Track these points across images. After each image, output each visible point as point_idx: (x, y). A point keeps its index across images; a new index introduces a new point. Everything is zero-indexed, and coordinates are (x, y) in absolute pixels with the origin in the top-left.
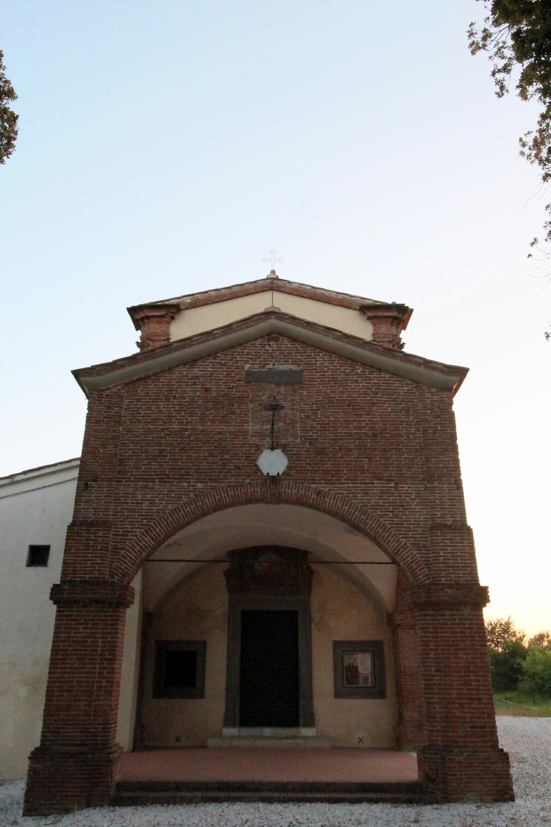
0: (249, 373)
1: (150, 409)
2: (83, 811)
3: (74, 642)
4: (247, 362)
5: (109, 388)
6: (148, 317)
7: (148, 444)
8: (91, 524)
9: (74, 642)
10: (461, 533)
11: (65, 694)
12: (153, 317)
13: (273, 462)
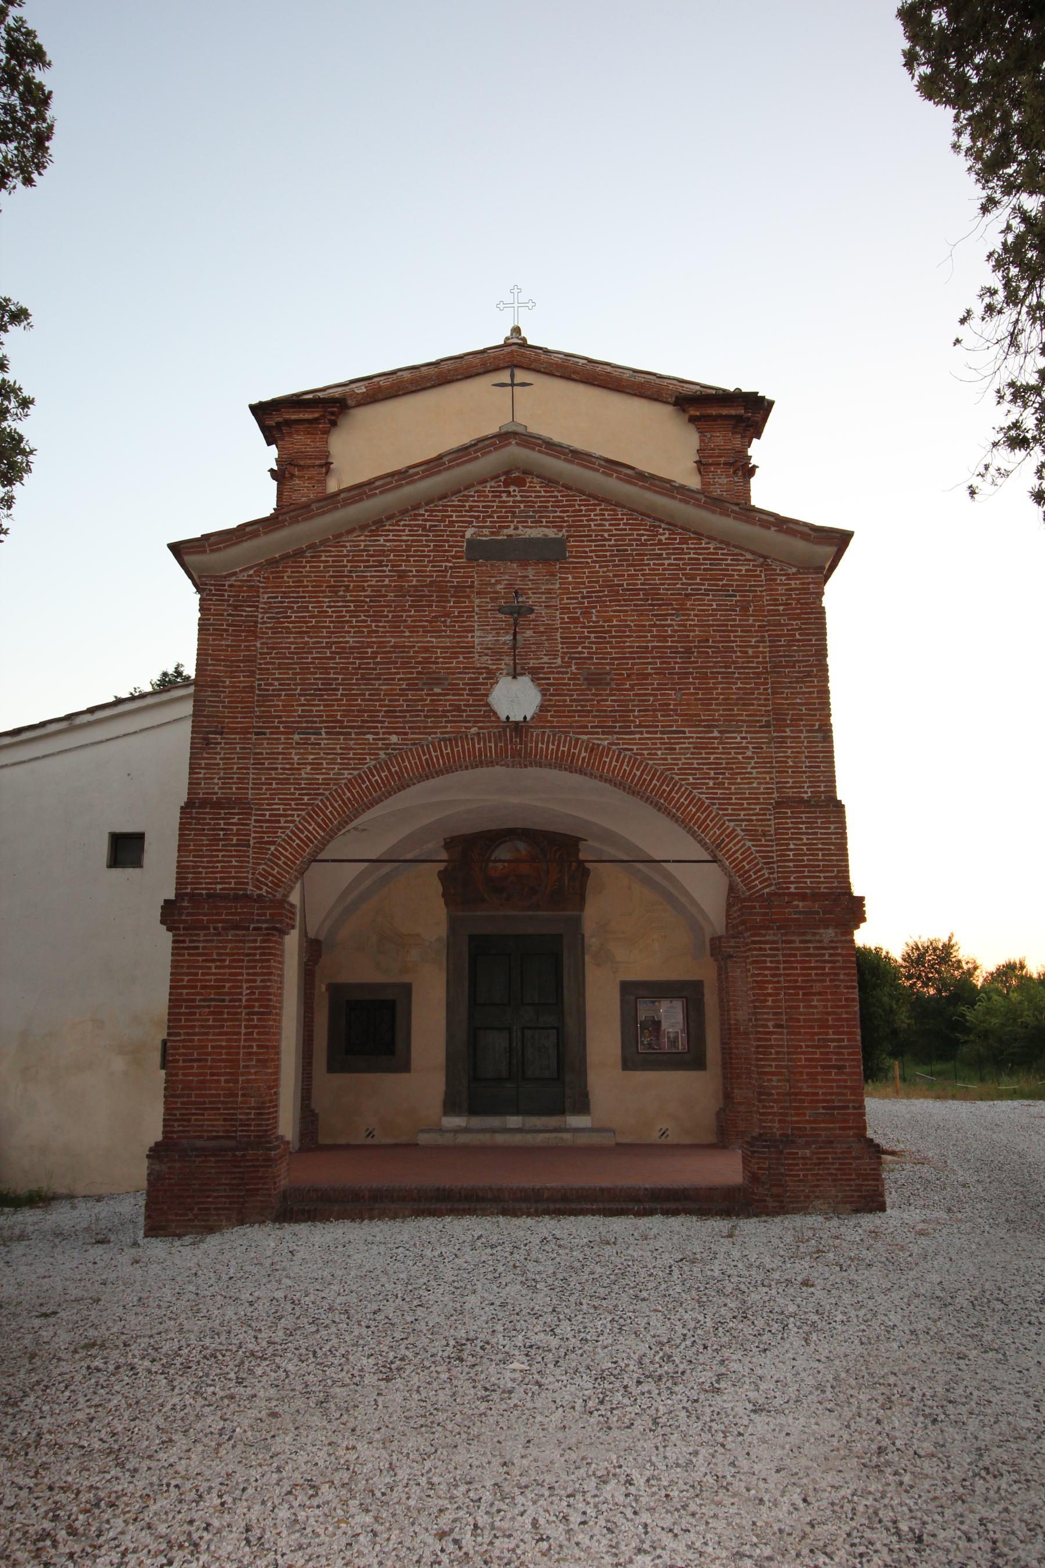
3: (204, 987)
5: (234, 574)
6: (288, 423)
7: (305, 670)
8: (218, 805)
9: (204, 987)
13: (515, 699)
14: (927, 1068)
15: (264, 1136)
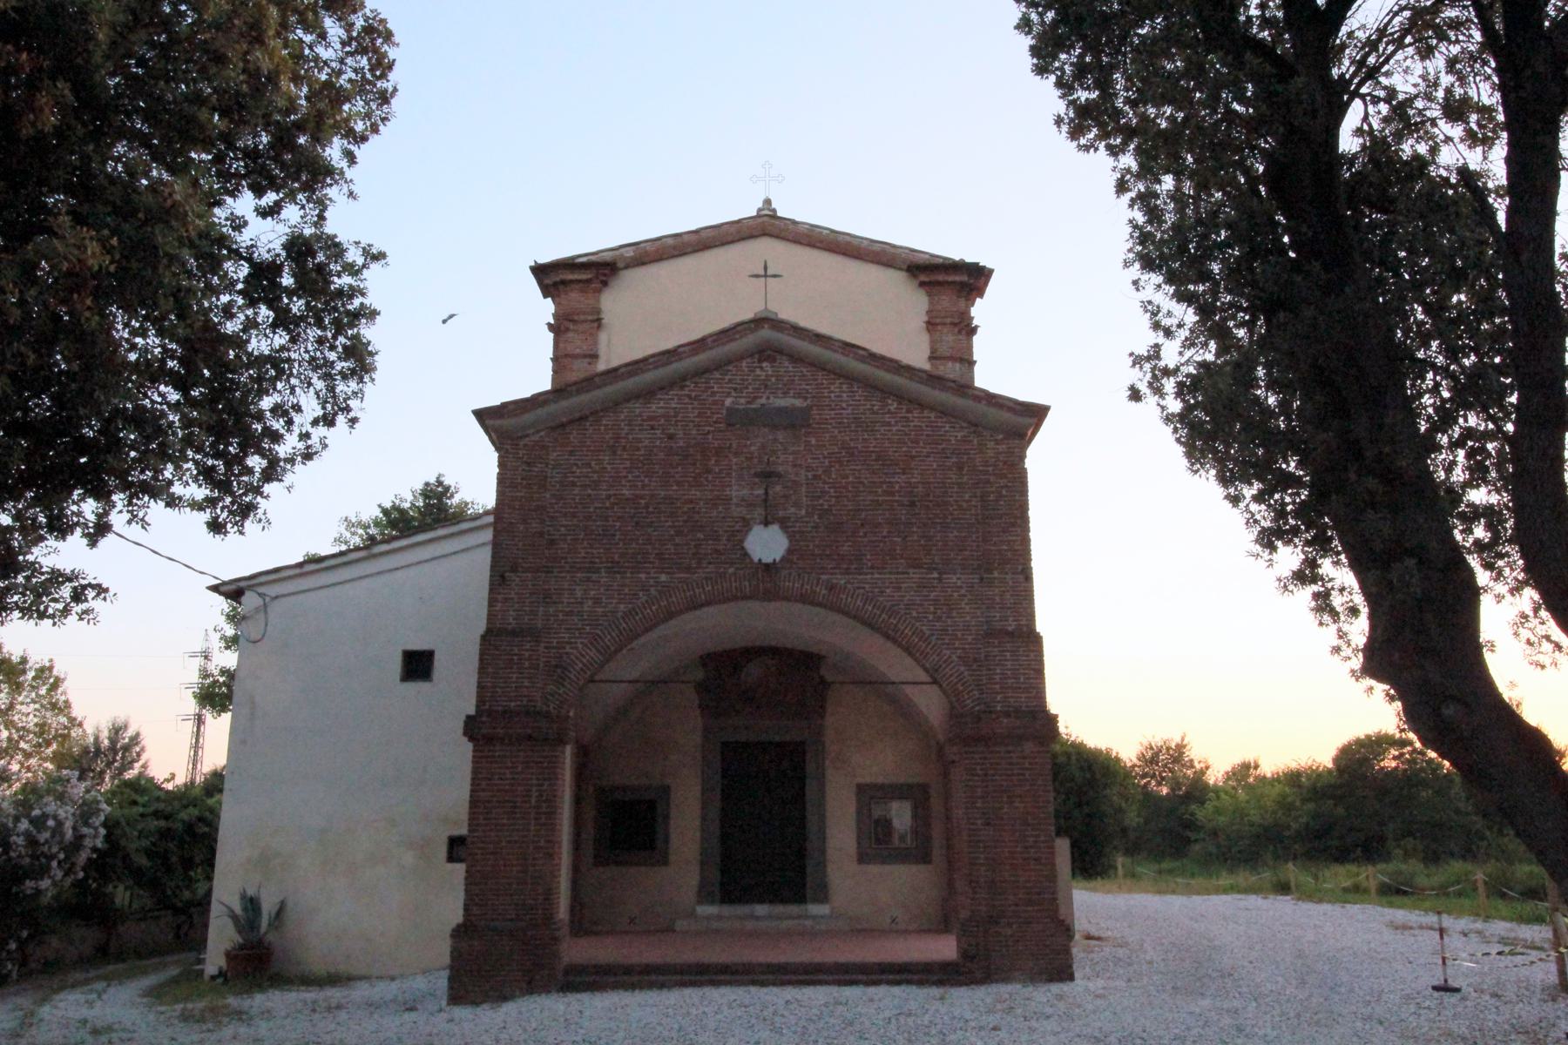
0: (731, 411)
1: (589, 465)
6: (563, 282)
8: (514, 633)
10: (1025, 643)
12: (572, 281)
13: (767, 544)
14: (1156, 867)
15: (549, 918)
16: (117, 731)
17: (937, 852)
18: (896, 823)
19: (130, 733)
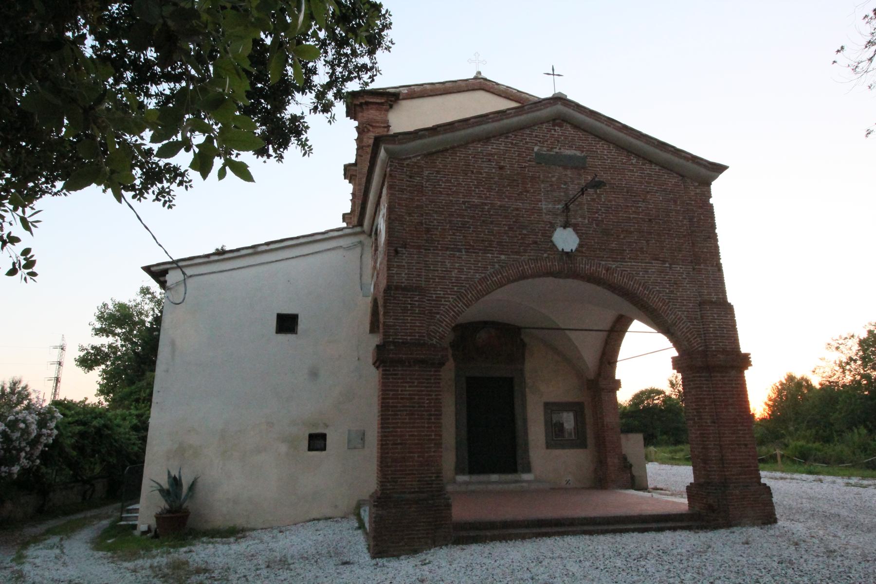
2: (432, 551)
3: (402, 399)
4: (536, 144)
5: (410, 158)
6: (367, 103)
7: (451, 215)
8: (405, 289)
9: (402, 399)
11: (399, 447)
13: (566, 240)
16: (14, 384)
17: (591, 441)
18: (566, 426)
19: (22, 385)
